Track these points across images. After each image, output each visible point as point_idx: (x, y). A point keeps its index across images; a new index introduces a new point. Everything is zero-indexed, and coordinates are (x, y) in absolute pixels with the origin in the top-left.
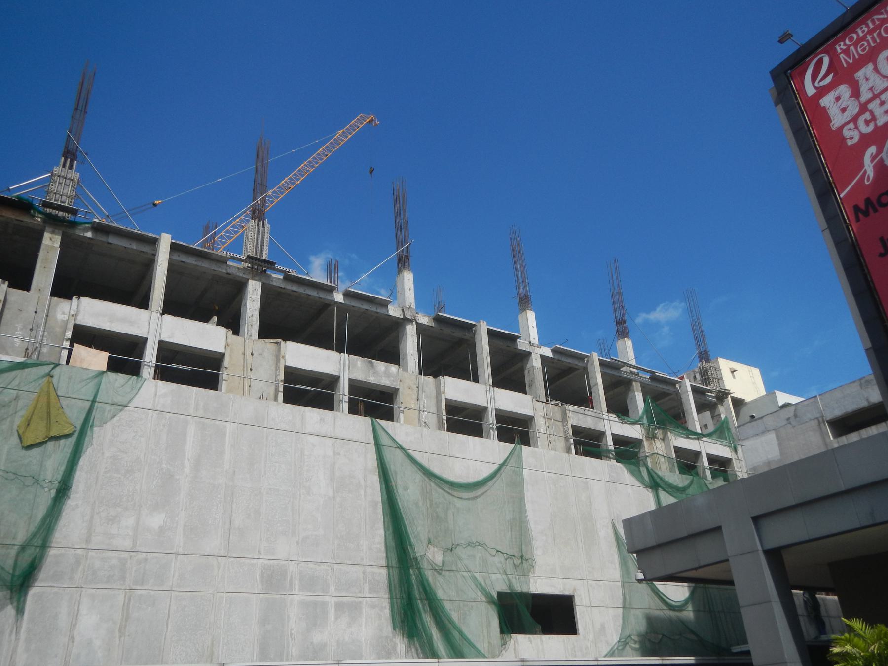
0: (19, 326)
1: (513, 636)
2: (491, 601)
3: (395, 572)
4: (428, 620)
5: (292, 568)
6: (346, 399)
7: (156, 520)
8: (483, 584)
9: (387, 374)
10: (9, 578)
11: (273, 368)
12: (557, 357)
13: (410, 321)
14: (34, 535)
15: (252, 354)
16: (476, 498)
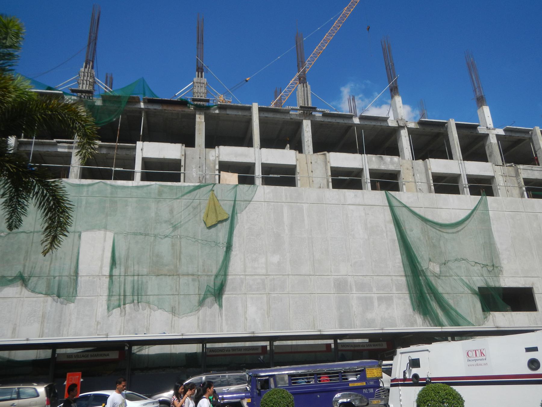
0: (194, 166)
1: (492, 313)
2: (474, 292)
3: (411, 279)
4: (434, 305)
5: (350, 279)
6: (369, 181)
7: (275, 259)
8: (468, 283)
9: (392, 163)
10: (213, 291)
11: (324, 169)
12: (508, 134)
13: (403, 127)
14: (220, 270)
15: (311, 163)
16: (458, 232)
